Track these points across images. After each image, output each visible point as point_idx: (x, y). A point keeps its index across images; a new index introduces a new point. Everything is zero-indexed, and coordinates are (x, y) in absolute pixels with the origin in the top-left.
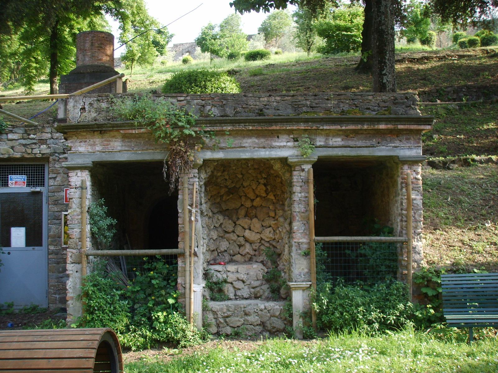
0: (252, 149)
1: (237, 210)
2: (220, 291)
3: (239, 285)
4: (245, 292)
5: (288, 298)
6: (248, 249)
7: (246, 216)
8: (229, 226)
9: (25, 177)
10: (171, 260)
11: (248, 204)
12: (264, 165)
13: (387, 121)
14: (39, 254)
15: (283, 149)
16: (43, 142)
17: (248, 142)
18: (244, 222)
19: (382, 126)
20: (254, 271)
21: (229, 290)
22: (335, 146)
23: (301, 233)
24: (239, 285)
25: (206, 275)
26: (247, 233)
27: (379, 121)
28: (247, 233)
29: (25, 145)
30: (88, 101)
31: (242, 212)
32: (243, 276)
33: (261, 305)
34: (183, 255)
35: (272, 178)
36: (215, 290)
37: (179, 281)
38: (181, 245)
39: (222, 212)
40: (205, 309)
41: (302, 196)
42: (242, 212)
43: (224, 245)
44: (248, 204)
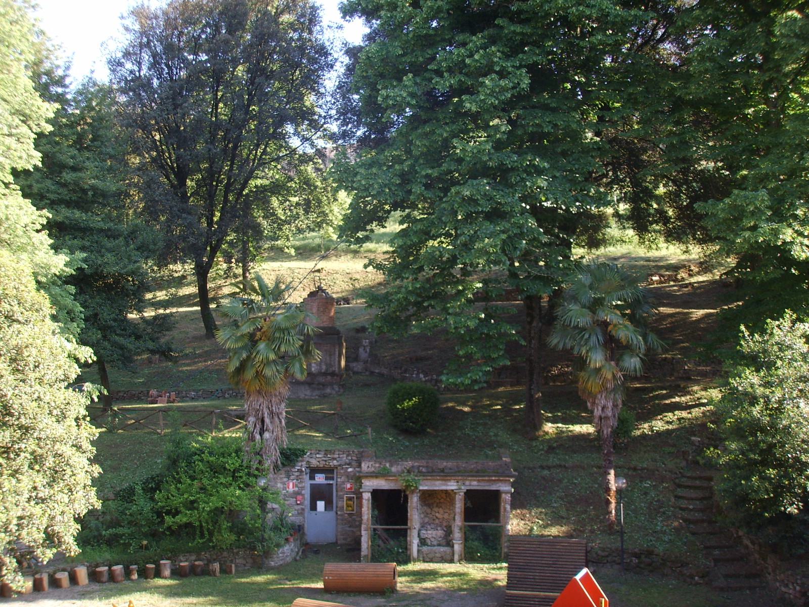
0: (438, 485)
1: (433, 504)
2: (425, 541)
3: (433, 540)
4: (435, 543)
5: (453, 547)
6: (437, 521)
7: (437, 506)
8: (429, 511)
9: (324, 475)
10: (406, 530)
11: (438, 501)
12: (446, 492)
13: (495, 476)
14: (331, 514)
15: (452, 486)
16: (334, 459)
17: (438, 483)
18: (436, 509)
19: (493, 478)
20: (440, 533)
21: (429, 542)
22: (474, 484)
23: (459, 521)
24: (433, 540)
25: (419, 536)
26: (437, 514)
27: (492, 476)
28: (437, 514)
29: (326, 461)
30: (371, 463)
31: (435, 505)
32: (434, 536)
33: (442, 549)
34: (410, 529)
35: (449, 496)
36: (423, 542)
37: (408, 539)
38: (409, 524)
39: (426, 505)
40: (418, 551)
41: (459, 506)
42: (435, 505)
43: (426, 520)
44: (438, 501)
